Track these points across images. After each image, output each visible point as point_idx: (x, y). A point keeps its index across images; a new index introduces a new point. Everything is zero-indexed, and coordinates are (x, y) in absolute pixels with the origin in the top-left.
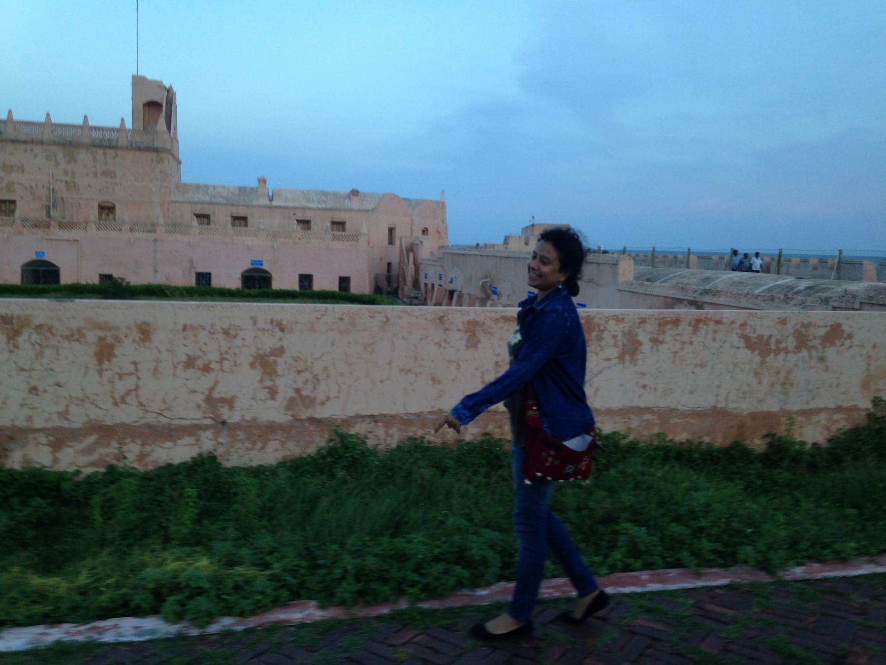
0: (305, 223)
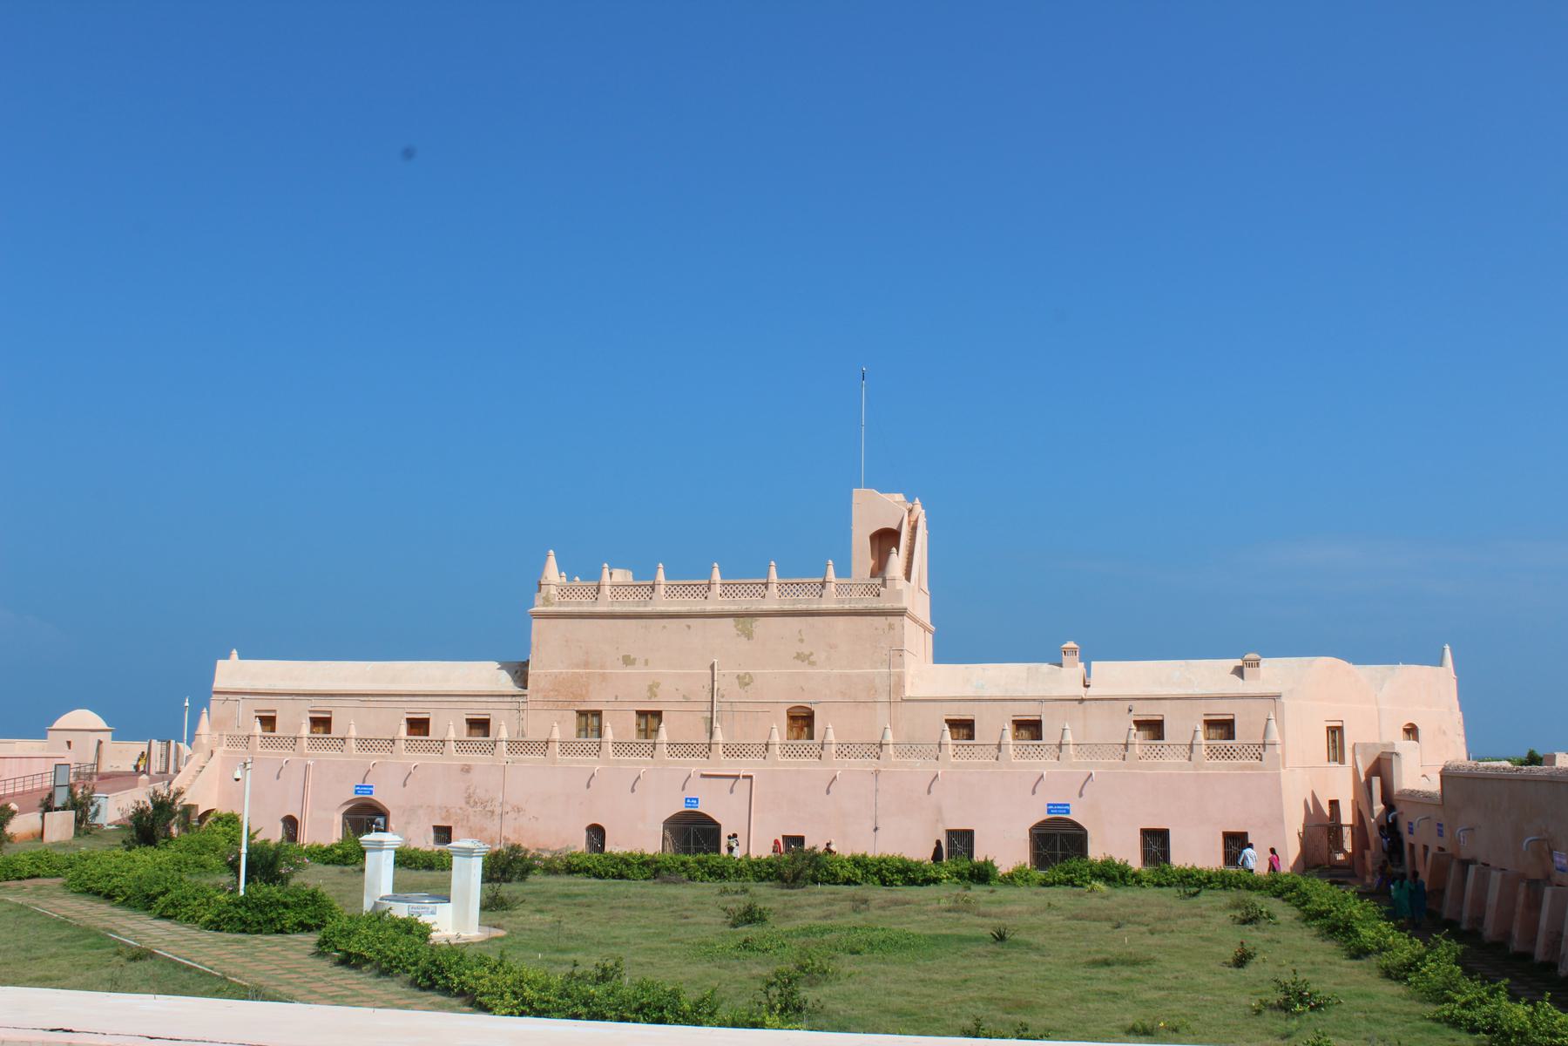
0: (1154, 728)
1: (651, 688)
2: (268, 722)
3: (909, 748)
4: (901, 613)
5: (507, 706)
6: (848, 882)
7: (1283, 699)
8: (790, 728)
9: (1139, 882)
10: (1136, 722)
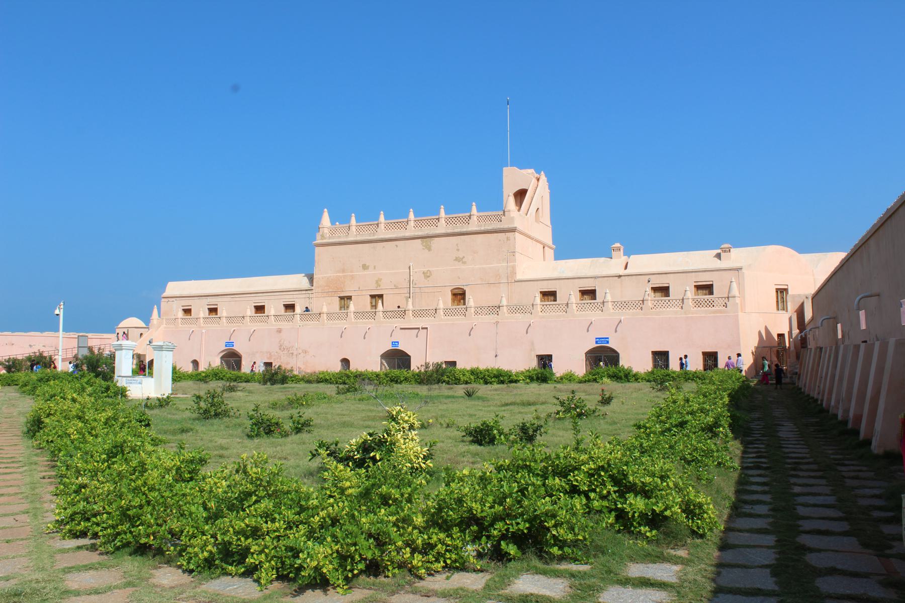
1: (377, 282)
2: (187, 311)
3: (516, 309)
4: (513, 230)
5: (304, 296)
6: (467, 383)
7: (743, 270)
8: (453, 300)
9: (636, 380)
10: (652, 288)
